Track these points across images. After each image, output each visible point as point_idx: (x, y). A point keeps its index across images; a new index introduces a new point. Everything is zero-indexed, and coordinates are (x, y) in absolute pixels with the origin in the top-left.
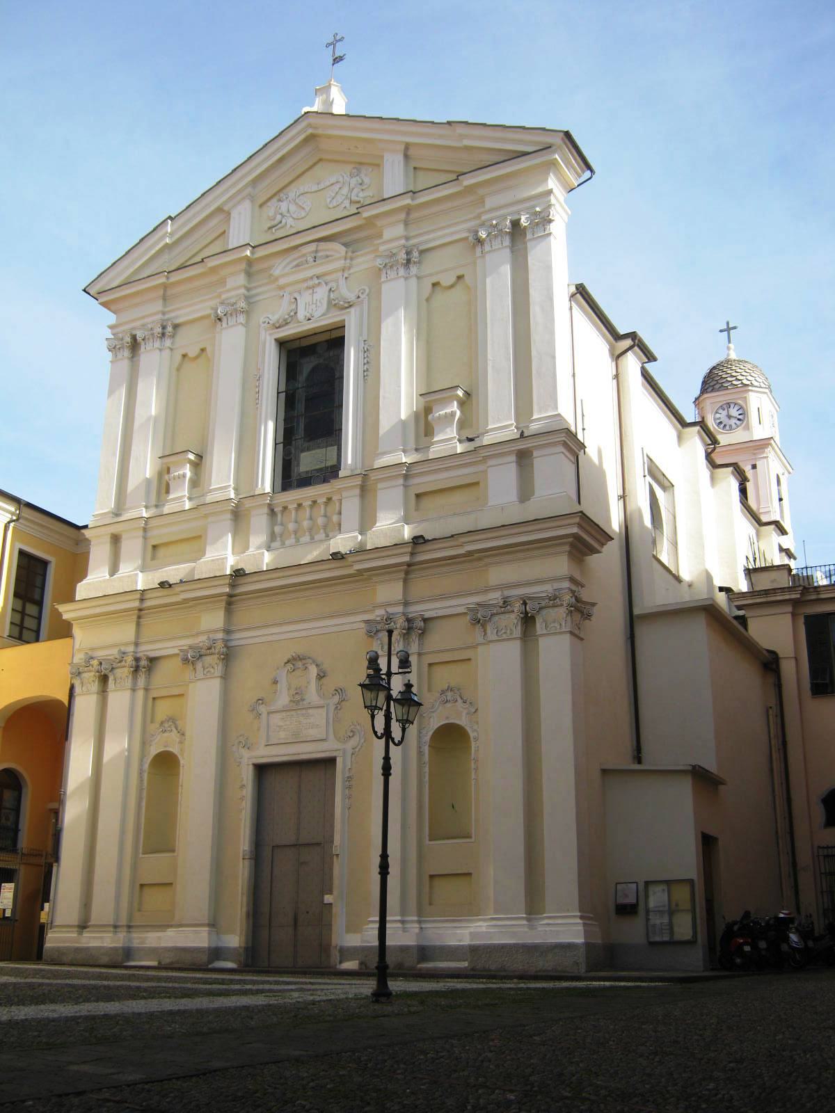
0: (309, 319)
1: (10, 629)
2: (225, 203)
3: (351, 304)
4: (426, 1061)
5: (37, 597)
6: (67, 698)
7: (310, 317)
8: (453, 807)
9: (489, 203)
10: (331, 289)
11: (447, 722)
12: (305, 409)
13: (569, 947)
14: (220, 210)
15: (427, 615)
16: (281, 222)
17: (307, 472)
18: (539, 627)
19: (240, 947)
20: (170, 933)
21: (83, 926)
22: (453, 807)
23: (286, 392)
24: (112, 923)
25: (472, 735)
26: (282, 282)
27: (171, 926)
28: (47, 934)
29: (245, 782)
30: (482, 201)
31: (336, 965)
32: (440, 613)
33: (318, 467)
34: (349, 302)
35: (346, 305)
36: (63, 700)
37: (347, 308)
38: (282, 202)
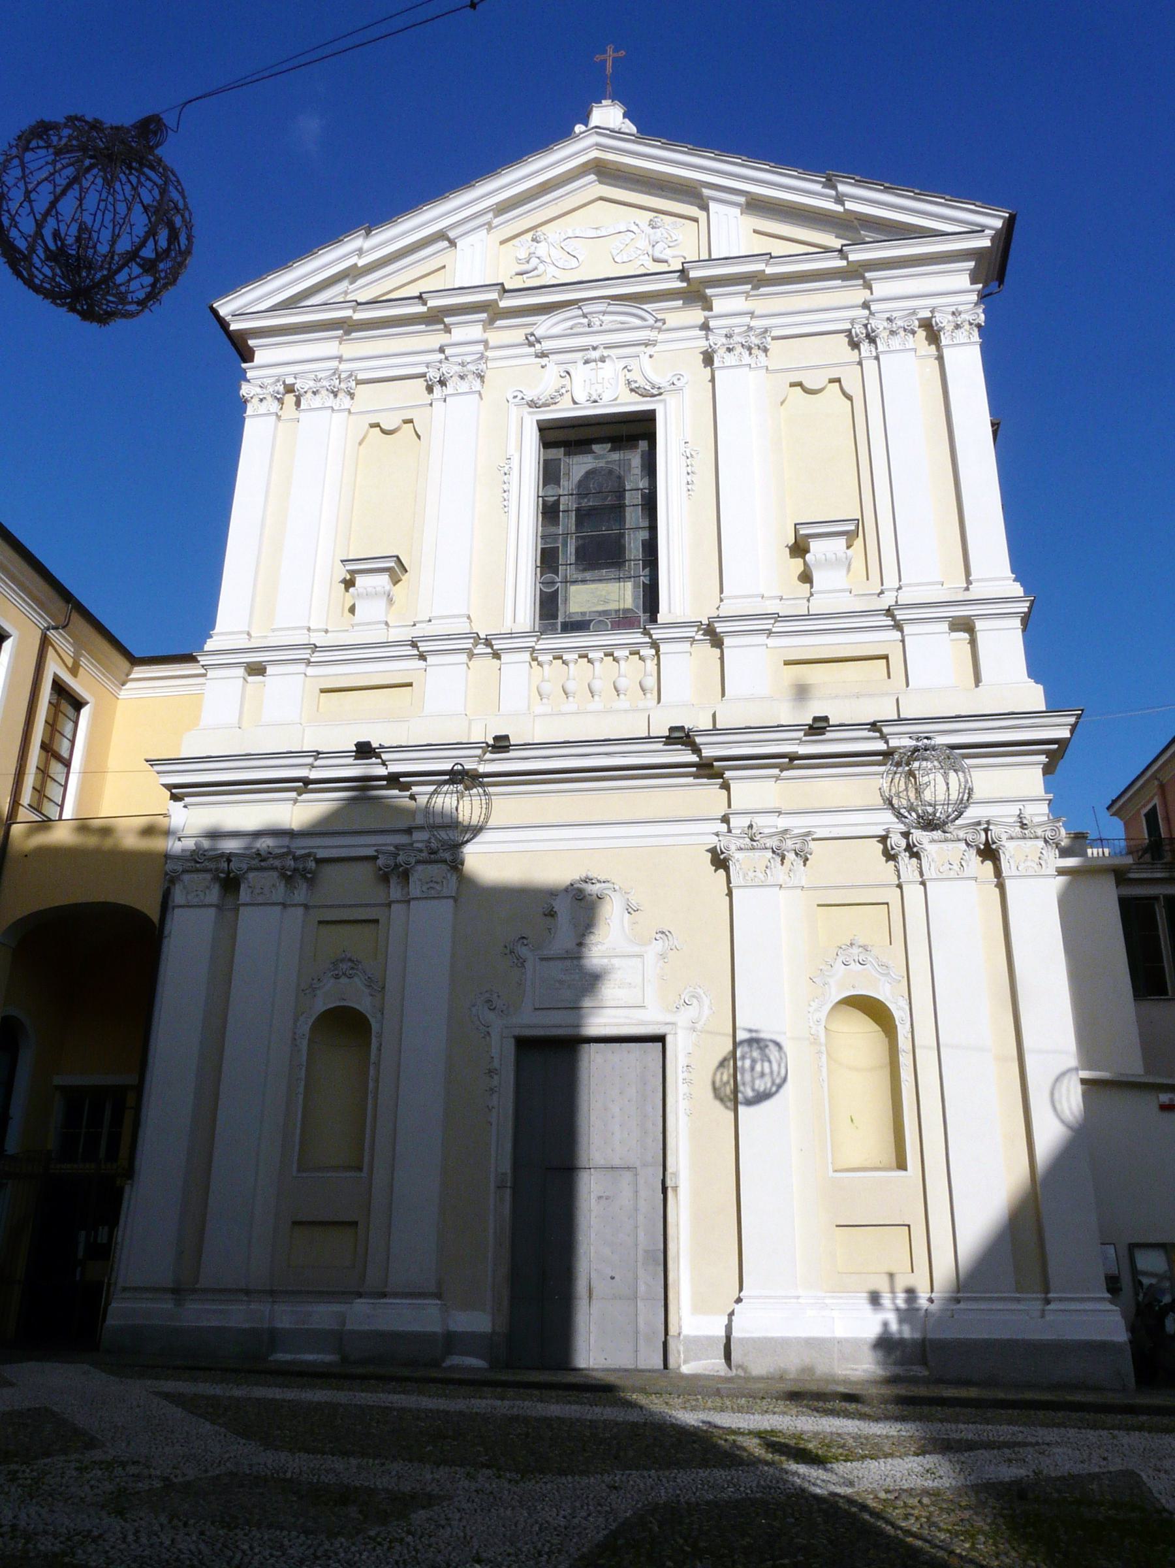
0: (595, 401)
1: (32, 796)
2: (453, 226)
3: (662, 391)
4: (589, 1515)
5: (66, 755)
6: (158, 909)
7: (598, 399)
8: (852, 1120)
9: (881, 289)
10: (626, 367)
11: (342, 1004)
12: (577, 526)
13: (1102, 1347)
14: (441, 236)
15: (321, 854)
16: (536, 269)
17: (583, 614)
18: (244, 895)
19: (493, 1333)
20: (361, 1306)
21: (178, 1292)
22: (852, 1120)
23: (625, 490)
24: (171, 1286)
25: (375, 1026)
26: (547, 345)
27: (360, 1295)
28: (108, 1304)
29: (496, 1064)
30: (448, 330)
31: (679, 1366)
32: (334, 853)
33: (600, 608)
34: (659, 388)
35: (655, 392)
36: (145, 910)
37: (654, 396)
38: (538, 242)
